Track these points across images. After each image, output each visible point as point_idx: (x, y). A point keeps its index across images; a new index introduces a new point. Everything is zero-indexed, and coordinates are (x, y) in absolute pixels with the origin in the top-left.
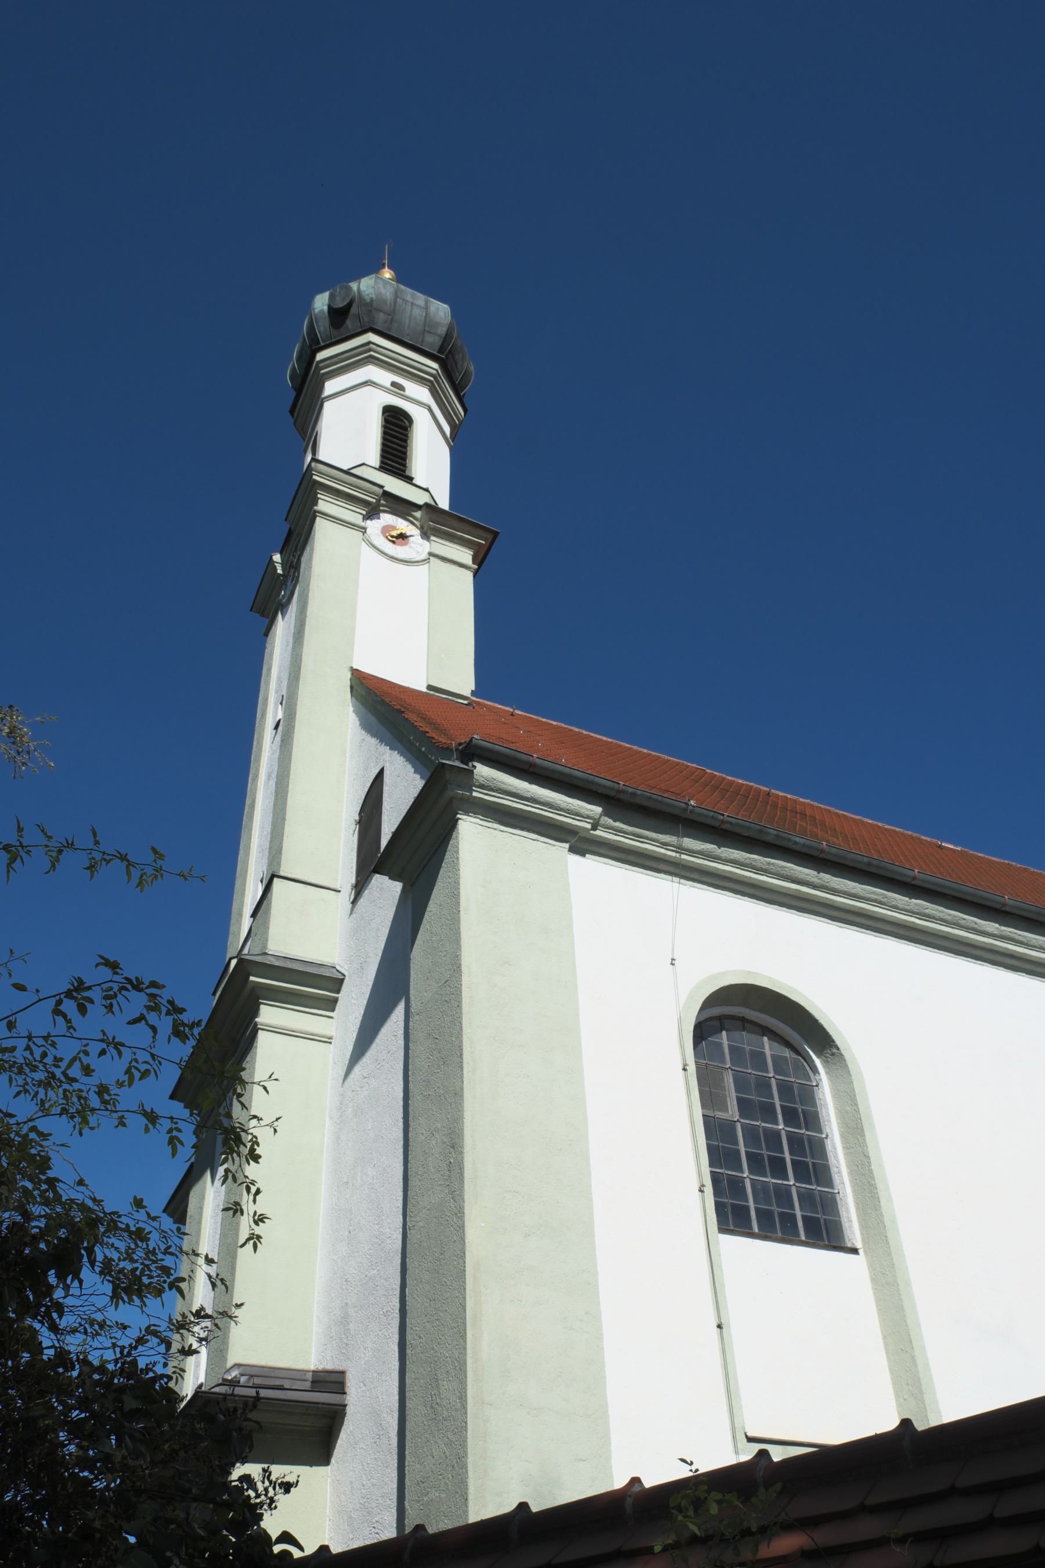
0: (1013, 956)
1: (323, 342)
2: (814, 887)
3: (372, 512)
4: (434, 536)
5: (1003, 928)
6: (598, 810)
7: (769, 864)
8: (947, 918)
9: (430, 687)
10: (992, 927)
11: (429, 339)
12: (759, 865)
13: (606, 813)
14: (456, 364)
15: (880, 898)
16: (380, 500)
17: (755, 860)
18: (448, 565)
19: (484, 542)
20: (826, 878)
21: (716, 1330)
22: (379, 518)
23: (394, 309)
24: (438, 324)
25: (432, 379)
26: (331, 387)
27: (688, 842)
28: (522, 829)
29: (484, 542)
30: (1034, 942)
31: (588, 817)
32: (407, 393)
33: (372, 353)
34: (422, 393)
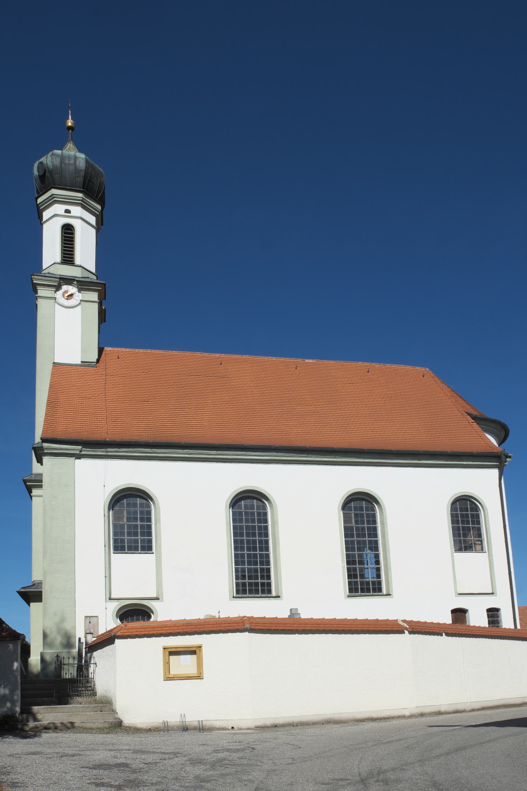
0: (223, 459)
2: (151, 453)
3: (58, 288)
4: (82, 291)
5: (218, 452)
6: (81, 447)
7: (135, 450)
8: (197, 453)
9: (82, 362)
11: (78, 180)
12: (132, 451)
13: (83, 447)
14: (94, 184)
15: (173, 452)
16: (60, 281)
17: (130, 450)
18: (88, 303)
19: (101, 288)
20: (154, 450)
21: (104, 578)
22: (61, 289)
23: (61, 170)
24: (81, 170)
25: (81, 202)
26: (46, 215)
27: (109, 450)
28: (63, 456)
29: (101, 288)
31: (78, 450)
32: (72, 214)
34: (77, 211)
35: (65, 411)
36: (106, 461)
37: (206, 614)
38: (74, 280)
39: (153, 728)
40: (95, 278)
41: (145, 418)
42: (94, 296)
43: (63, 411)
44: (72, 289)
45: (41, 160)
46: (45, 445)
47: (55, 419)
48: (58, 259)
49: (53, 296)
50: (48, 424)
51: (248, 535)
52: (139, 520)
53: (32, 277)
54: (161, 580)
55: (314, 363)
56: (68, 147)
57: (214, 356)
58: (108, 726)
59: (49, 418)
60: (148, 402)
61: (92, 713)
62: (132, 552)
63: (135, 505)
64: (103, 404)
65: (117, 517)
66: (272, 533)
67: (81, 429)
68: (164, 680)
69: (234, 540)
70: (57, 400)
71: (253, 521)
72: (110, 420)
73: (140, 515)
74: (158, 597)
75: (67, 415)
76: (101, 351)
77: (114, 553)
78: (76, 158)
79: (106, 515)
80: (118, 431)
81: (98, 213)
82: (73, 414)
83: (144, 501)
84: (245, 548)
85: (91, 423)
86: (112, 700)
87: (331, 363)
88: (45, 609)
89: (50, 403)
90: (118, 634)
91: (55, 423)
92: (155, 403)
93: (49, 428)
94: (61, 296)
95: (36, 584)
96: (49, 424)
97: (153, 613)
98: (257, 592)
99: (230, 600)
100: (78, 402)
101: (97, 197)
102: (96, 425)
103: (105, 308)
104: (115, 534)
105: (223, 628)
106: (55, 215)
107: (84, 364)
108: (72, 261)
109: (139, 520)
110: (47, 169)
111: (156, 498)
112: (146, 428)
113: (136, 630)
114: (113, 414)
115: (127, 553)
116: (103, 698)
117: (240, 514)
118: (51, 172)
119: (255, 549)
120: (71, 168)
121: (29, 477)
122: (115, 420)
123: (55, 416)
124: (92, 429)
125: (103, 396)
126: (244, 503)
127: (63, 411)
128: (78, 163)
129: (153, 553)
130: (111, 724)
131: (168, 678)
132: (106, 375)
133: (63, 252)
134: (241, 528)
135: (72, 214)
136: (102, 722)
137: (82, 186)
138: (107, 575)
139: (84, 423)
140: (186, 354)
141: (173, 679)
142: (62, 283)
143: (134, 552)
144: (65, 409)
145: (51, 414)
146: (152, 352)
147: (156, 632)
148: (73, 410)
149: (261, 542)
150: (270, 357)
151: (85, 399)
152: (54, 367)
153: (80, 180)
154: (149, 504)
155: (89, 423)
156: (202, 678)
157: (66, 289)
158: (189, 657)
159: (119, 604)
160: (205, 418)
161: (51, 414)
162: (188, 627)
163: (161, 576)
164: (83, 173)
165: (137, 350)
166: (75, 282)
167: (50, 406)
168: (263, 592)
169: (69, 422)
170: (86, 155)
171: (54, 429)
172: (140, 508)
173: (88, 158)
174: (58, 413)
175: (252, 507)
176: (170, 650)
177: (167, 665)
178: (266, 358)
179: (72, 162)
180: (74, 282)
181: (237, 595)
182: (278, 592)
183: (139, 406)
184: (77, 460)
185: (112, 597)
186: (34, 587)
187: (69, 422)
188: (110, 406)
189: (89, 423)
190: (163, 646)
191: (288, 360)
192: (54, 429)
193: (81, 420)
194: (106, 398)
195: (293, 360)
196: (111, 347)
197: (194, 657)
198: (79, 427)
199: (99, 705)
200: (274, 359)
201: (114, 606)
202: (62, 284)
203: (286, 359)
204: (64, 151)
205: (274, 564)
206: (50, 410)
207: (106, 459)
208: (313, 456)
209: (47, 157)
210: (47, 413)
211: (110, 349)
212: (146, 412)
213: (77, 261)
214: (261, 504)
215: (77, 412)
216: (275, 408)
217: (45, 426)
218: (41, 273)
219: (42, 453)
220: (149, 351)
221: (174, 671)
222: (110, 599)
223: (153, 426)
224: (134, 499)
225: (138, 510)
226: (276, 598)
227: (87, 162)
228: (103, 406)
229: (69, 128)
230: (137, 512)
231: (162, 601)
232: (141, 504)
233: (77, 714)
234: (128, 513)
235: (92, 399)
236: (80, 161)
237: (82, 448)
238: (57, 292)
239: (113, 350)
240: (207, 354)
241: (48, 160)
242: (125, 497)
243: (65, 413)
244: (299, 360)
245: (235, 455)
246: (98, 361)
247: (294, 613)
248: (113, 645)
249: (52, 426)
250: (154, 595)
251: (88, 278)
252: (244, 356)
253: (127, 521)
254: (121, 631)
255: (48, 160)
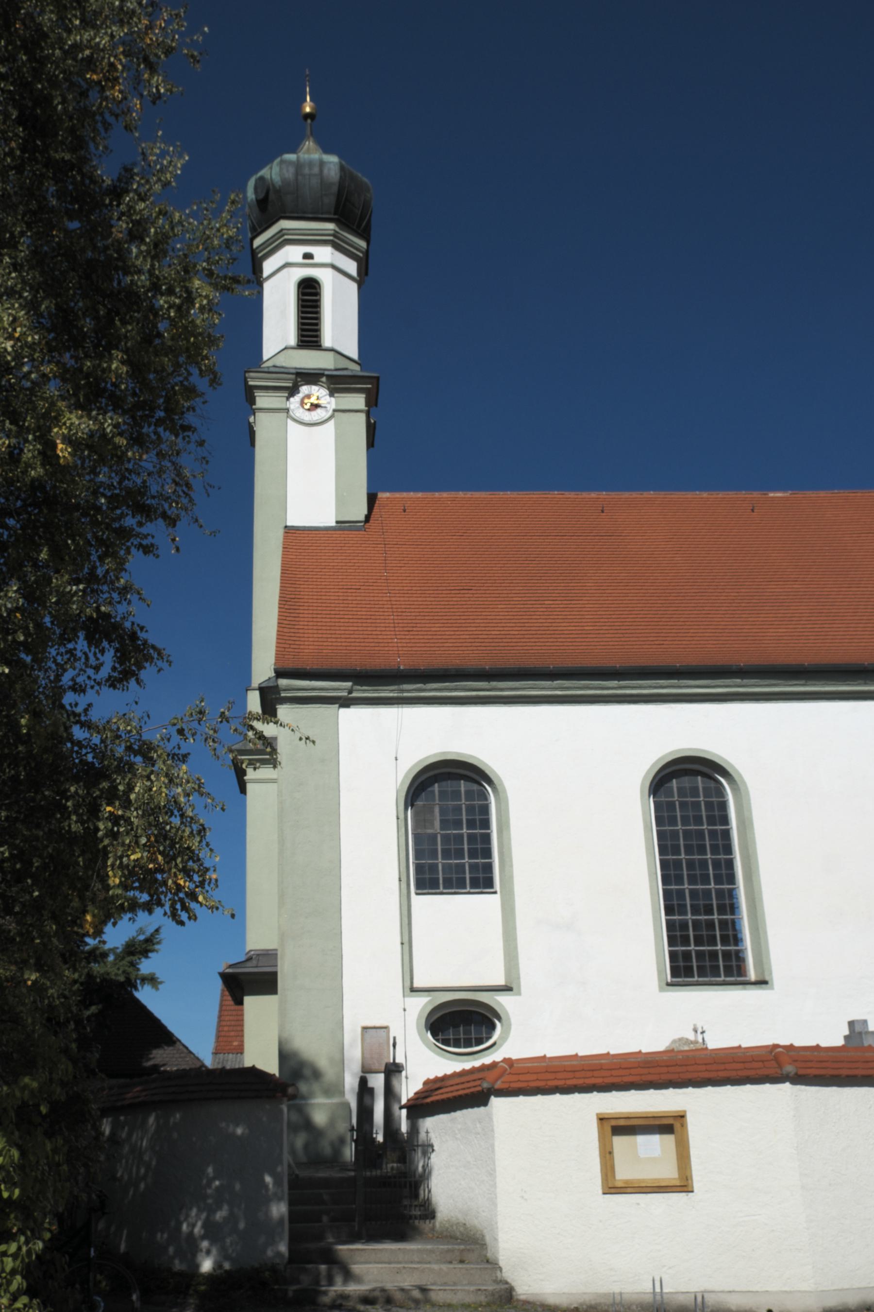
1: (260, 228)
3: (293, 391)
5: (621, 682)
6: (349, 684)
7: (457, 685)
8: (580, 686)
9: (337, 522)
10: (614, 683)
12: (451, 687)
13: (355, 684)
19: (370, 386)
25: (331, 238)
26: (269, 266)
27: (405, 686)
29: (370, 386)
30: (645, 685)
31: (345, 689)
32: (317, 259)
33: (286, 237)
34: (324, 253)
35: (315, 616)
36: (400, 709)
37: (677, 1036)
38: (322, 375)
39: (585, 1307)
40: (357, 368)
41: (468, 621)
42: (358, 401)
43: (310, 616)
44: (318, 393)
45: (261, 173)
46: (283, 682)
47: (296, 631)
48: (292, 340)
49: (283, 406)
50: (284, 641)
51: (689, 850)
52: (465, 826)
53: (247, 375)
54: (516, 948)
55: (787, 499)
56: (306, 147)
57: (587, 496)
58: (486, 1300)
59: (285, 630)
60: (470, 592)
61: (444, 1267)
62: (453, 891)
63: (456, 795)
64: (384, 599)
65: (418, 822)
66: (740, 844)
67: (348, 648)
68: (604, 1194)
69: (661, 861)
70: (297, 596)
71: (698, 820)
72: (401, 629)
73: (467, 815)
74: (509, 985)
75: (319, 624)
76: (372, 499)
77: (417, 894)
78: (322, 164)
79: (402, 816)
80: (420, 649)
81: (361, 255)
82: (329, 620)
83: (475, 787)
84: (685, 877)
85: (366, 636)
86: (483, 1236)
87: (822, 495)
88: (283, 1013)
89: (284, 603)
90: (498, 1085)
91: (298, 639)
92: (483, 592)
93: (286, 650)
94: (298, 405)
95: (254, 957)
96: (287, 642)
97: (499, 1018)
98: (715, 972)
99: (661, 989)
100: (337, 598)
101: (359, 226)
102: (376, 641)
103: (375, 422)
104: (418, 854)
105: (733, 1074)
106: (287, 265)
107: (342, 525)
108: (317, 342)
109: (465, 826)
110: (271, 187)
111: (500, 780)
112: (473, 641)
113: (534, 1077)
114: (405, 618)
115: (442, 893)
116: (455, 1228)
117: (671, 806)
118: (278, 191)
119: (705, 880)
120: (315, 182)
121: (241, 744)
122: (411, 629)
123: (296, 627)
124: (369, 648)
125: (383, 584)
126: (677, 783)
127: (310, 616)
128: (326, 171)
129: (495, 893)
130: (493, 1294)
131: (612, 1187)
132: (385, 544)
133: (300, 326)
134: (675, 835)
135: (317, 259)
136: (473, 1291)
137: (332, 211)
138: (406, 940)
139: (352, 636)
140: (531, 496)
141: (622, 1190)
142: (300, 382)
143: (457, 890)
144: (315, 612)
145: (288, 622)
146: (466, 496)
147: (580, 1082)
148: (329, 612)
149: (717, 864)
150: (698, 493)
151: (349, 591)
152: (287, 535)
153: (330, 201)
154: (484, 793)
155: (361, 636)
156: (690, 1190)
157: (307, 392)
158: (655, 1140)
159: (429, 1002)
160: (587, 617)
161: (288, 622)
162: (652, 1070)
163: (515, 939)
164: (335, 189)
165: (437, 494)
166: (324, 379)
167: (286, 607)
168: (729, 972)
169: (324, 636)
170: (340, 157)
171: (296, 650)
172: (466, 800)
173: (344, 163)
174: (302, 619)
175: (695, 792)
176: (614, 1123)
177: (607, 1156)
178: (689, 495)
179: (316, 170)
180: (322, 377)
181: (674, 980)
182: (763, 973)
183: (454, 599)
184: (343, 711)
185: (417, 984)
186: (249, 964)
187: (324, 636)
188: (398, 603)
189: (361, 636)
190: (597, 1115)
191: (734, 496)
192: (296, 650)
193: (347, 632)
194: (390, 588)
195: (743, 494)
196: (422, 491)
197: (670, 1139)
198: (344, 644)
199: (456, 1247)
200: (705, 495)
201: (420, 1005)
202: (299, 384)
203: (730, 493)
204: (301, 155)
205: (749, 910)
206: (285, 614)
207: (400, 706)
208: (817, 683)
209: (271, 168)
210: (282, 621)
211: (388, 495)
212: (469, 610)
213: (327, 340)
214: (712, 784)
215: (337, 616)
216: (722, 591)
217: (279, 645)
218: (260, 367)
219: (276, 699)
220: (461, 494)
221: (622, 1174)
222: (413, 990)
223: (486, 636)
224: (455, 783)
225: (464, 806)
226: (758, 986)
227: (342, 168)
228: (386, 603)
229: (307, 116)
230: (461, 809)
231: (519, 994)
232: (468, 792)
233: (411, 1268)
234: (442, 812)
235: (363, 591)
236: (329, 169)
237: (352, 687)
238: (292, 399)
239: (393, 496)
240: (571, 495)
241: (273, 172)
242: (436, 779)
243: (315, 620)
244: (756, 494)
245: (655, 687)
246: (368, 518)
247: (860, 1030)
248: (482, 1109)
249: (292, 646)
250: (501, 981)
251: (346, 369)
252: (645, 493)
253: (442, 829)
254: (503, 1079)
255: (273, 172)
